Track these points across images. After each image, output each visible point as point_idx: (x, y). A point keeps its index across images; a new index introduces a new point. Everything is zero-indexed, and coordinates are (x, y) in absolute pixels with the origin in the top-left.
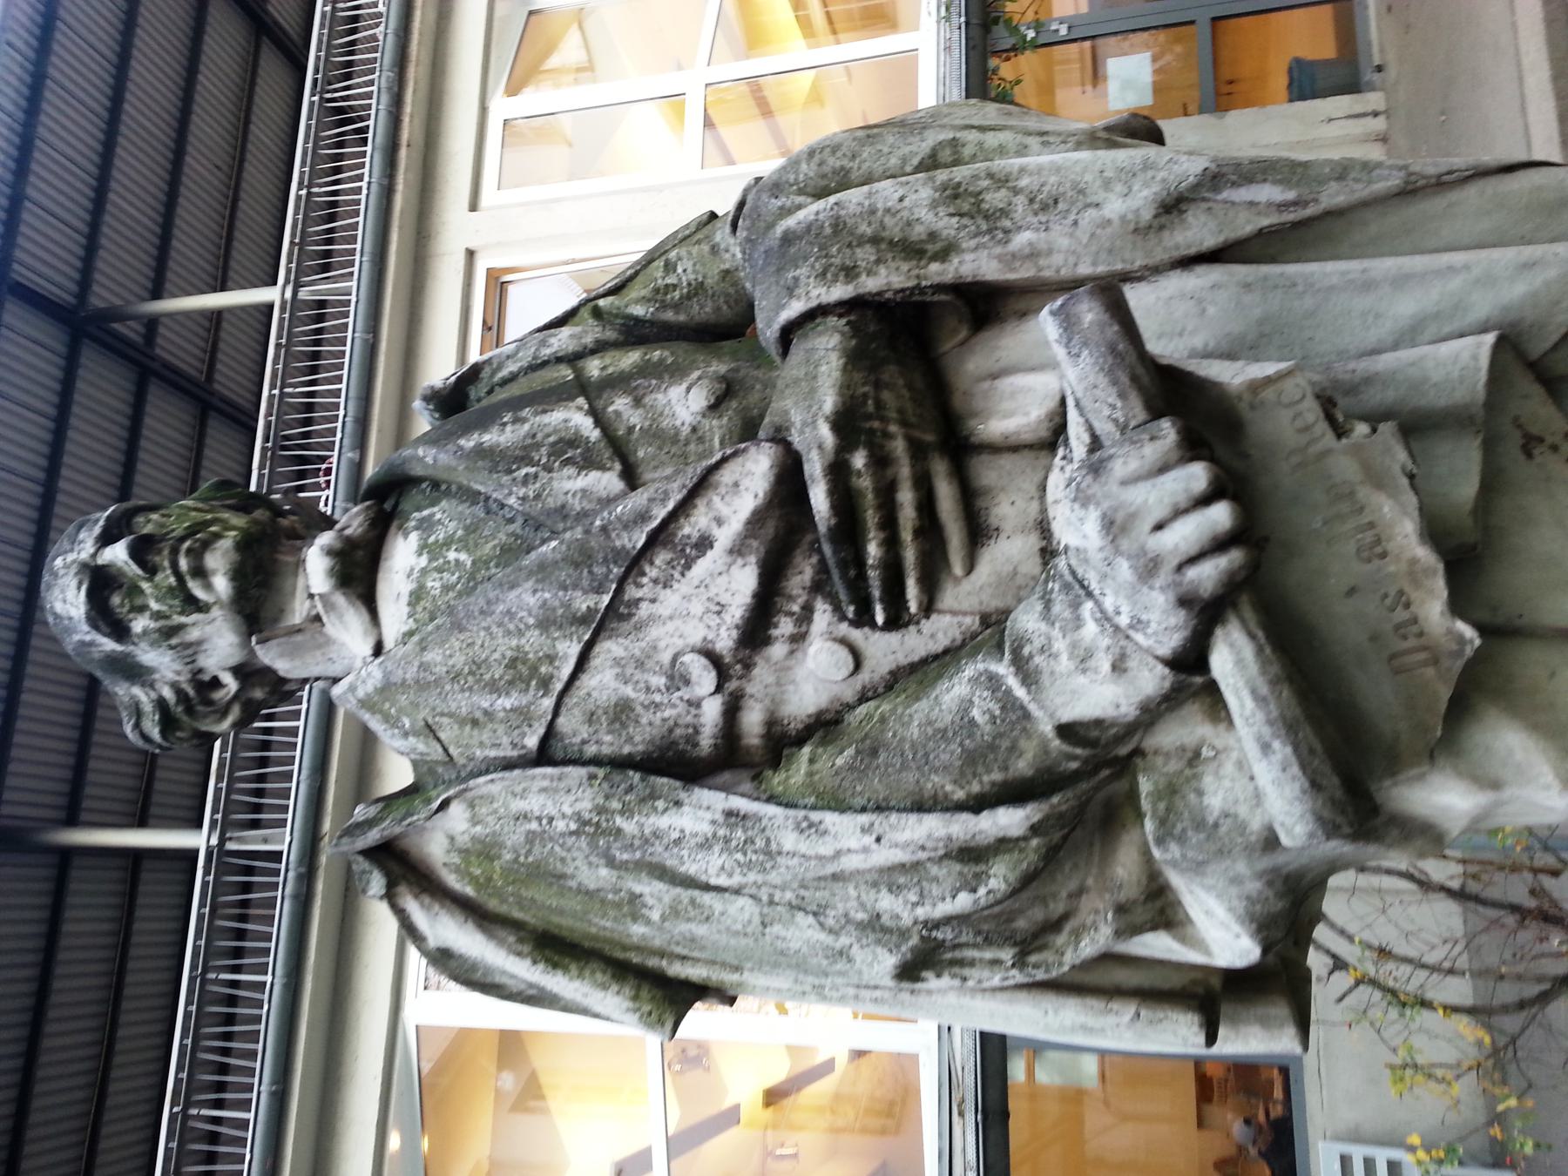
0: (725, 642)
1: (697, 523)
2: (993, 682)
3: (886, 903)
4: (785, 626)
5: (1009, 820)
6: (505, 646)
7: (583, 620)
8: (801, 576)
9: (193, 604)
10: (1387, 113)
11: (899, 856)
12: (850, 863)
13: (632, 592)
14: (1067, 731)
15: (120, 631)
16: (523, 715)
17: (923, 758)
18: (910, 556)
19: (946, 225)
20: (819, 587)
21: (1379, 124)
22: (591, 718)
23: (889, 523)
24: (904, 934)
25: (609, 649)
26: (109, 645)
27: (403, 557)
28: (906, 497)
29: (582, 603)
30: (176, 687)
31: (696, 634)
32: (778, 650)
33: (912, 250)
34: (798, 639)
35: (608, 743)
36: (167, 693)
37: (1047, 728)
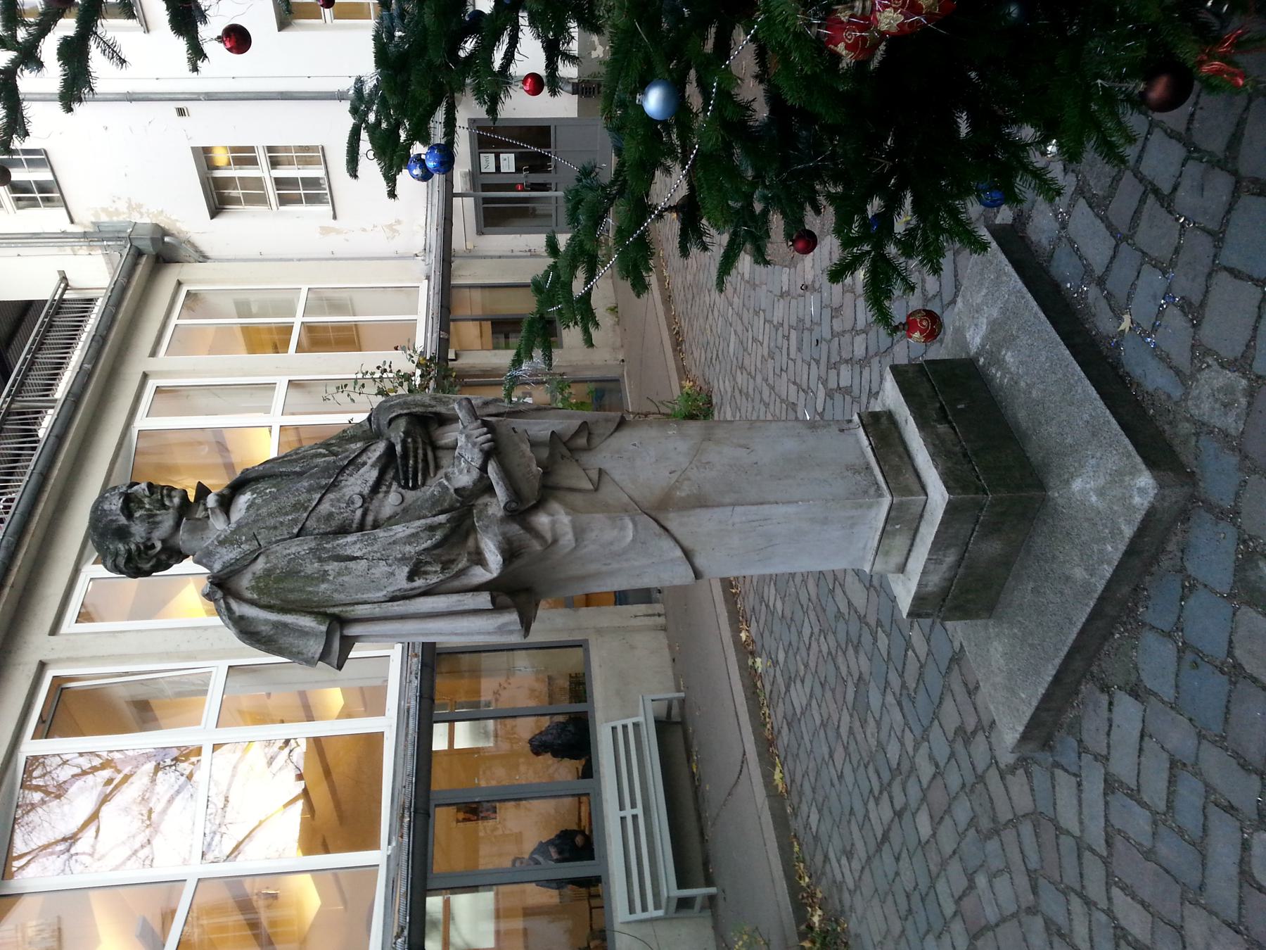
0: (366, 491)
1: (364, 458)
2: (440, 484)
3: (408, 548)
4: (384, 488)
5: (442, 518)
6: (293, 500)
7: (323, 487)
8: (391, 474)
9: (164, 507)
10: (665, 615)
11: (413, 531)
12: (399, 536)
13: (340, 478)
14: (456, 490)
15: (130, 516)
16: (295, 521)
17: (421, 507)
18: (420, 466)
19: (433, 403)
20: (394, 478)
21: (661, 620)
22: (318, 520)
23: (416, 457)
24: (411, 558)
25: (331, 496)
26: (123, 520)
27: (244, 500)
28: (420, 452)
29: (323, 482)
30: (138, 547)
31: (357, 490)
32: (381, 495)
33: (423, 405)
34: (387, 492)
35: (323, 528)
36: (133, 547)
37: (452, 491)
